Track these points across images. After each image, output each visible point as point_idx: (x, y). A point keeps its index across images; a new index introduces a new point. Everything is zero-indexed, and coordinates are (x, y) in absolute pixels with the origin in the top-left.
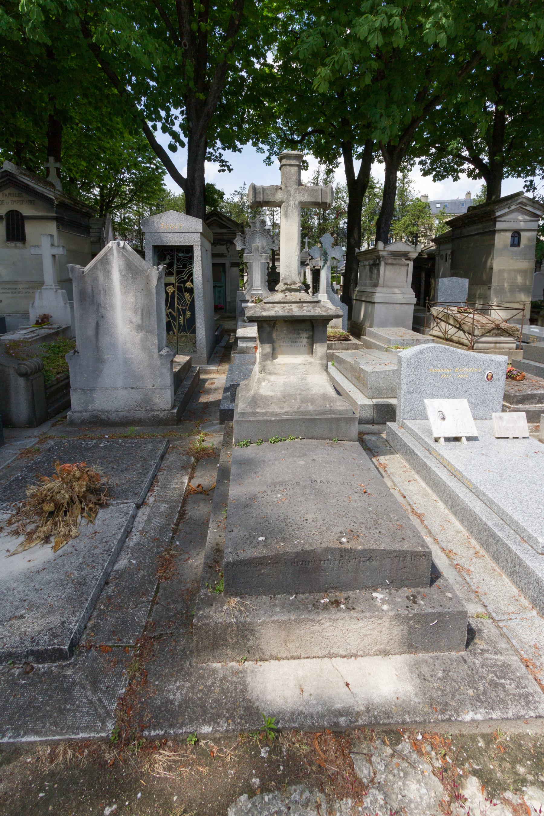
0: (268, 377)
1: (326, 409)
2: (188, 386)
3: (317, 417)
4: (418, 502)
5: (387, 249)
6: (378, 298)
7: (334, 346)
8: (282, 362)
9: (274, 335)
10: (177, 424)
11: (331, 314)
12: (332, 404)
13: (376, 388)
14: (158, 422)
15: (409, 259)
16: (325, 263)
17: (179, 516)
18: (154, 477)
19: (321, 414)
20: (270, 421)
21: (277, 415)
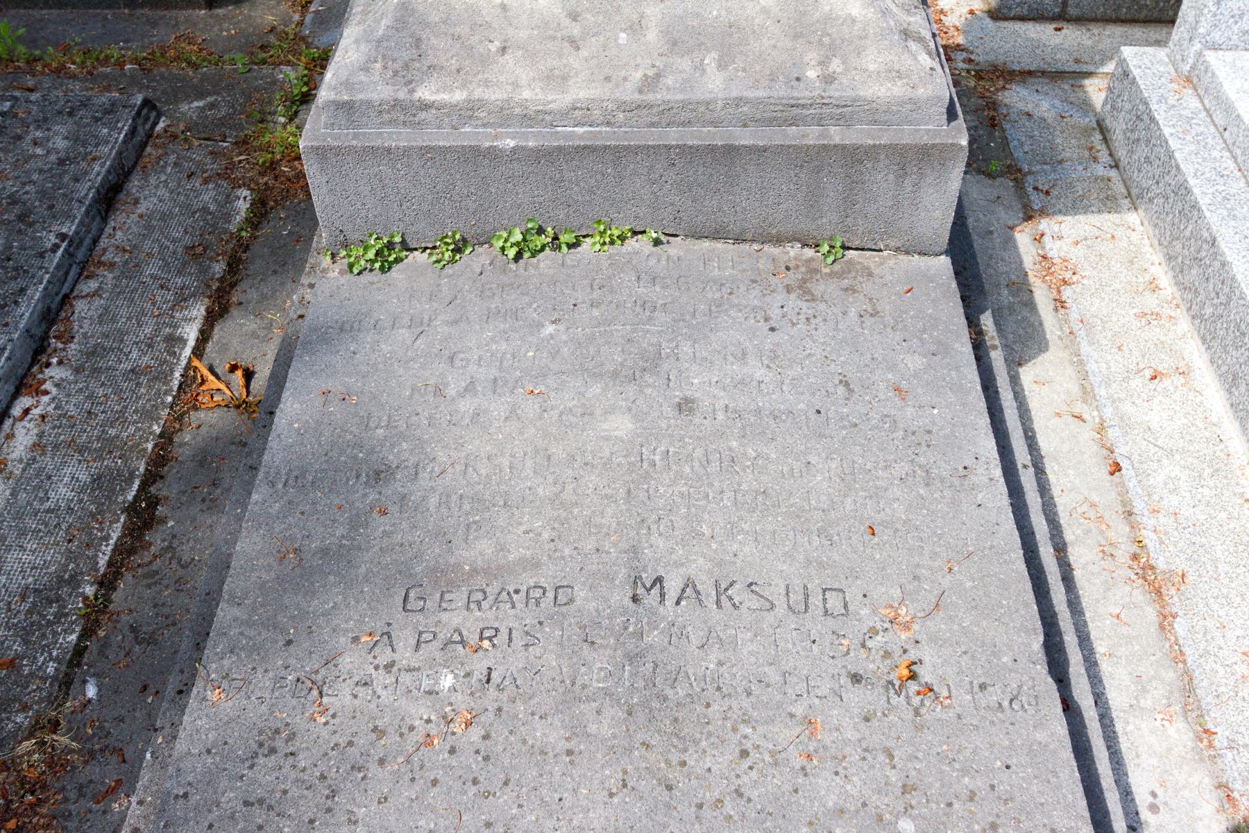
1: (801, 93)
3: (745, 138)
4: (1172, 501)
12: (836, 65)
17: (129, 531)
18: (54, 314)
19: (771, 122)
20: (493, 154)
21: (528, 119)
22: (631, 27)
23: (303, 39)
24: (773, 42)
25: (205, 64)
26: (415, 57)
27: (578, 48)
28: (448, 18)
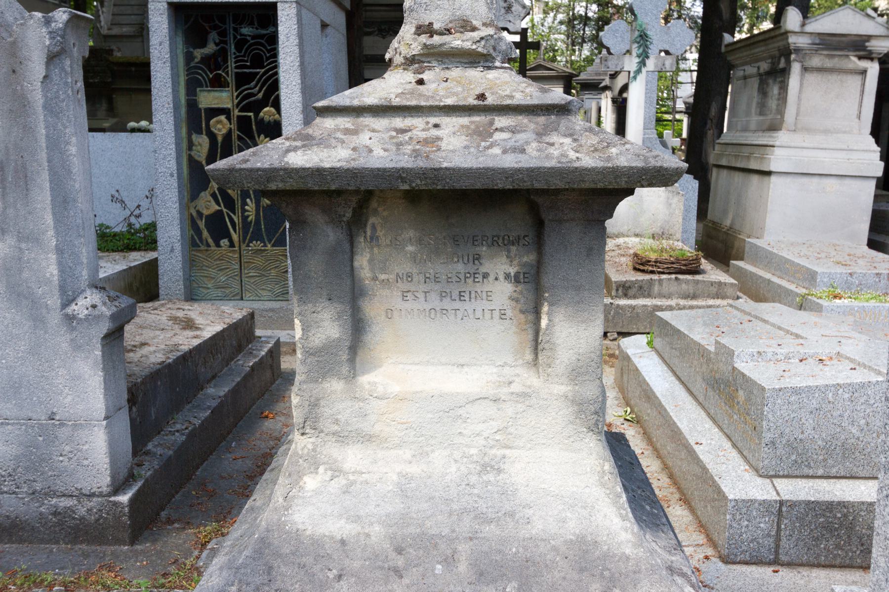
0: (332, 450)
2: (214, 404)
5: (809, 28)
6: (777, 161)
7: (656, 288)
8: (395, 388)
9: (362, 261)
10: (132, 543)
11: (623, 162)
13: (789, 444)
14: (77, 532)
15: (869, 57)
16: (643, 63)
19: (736, 49)
22: (445, 560)
23: (197, 569)
24: (562, 574)
25: (116, 587)
26: (266, 581)
27: (401, 577)
28: (297, 550)
